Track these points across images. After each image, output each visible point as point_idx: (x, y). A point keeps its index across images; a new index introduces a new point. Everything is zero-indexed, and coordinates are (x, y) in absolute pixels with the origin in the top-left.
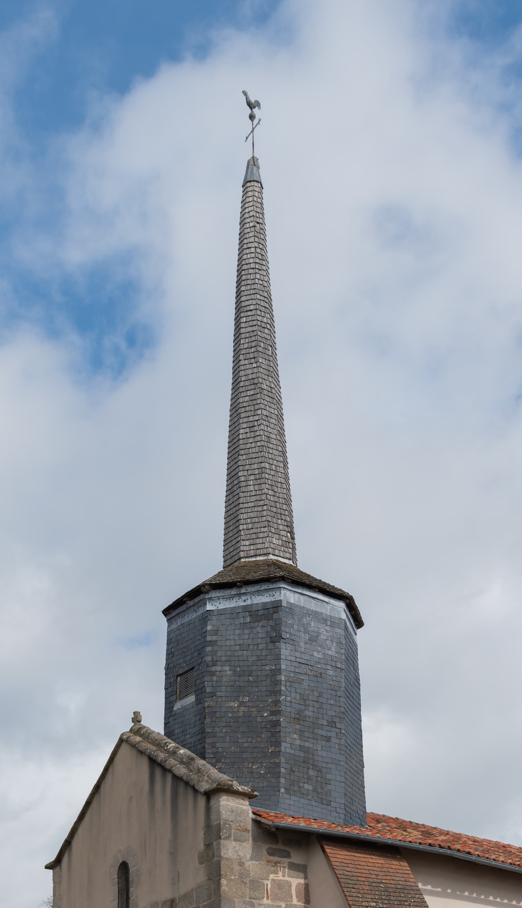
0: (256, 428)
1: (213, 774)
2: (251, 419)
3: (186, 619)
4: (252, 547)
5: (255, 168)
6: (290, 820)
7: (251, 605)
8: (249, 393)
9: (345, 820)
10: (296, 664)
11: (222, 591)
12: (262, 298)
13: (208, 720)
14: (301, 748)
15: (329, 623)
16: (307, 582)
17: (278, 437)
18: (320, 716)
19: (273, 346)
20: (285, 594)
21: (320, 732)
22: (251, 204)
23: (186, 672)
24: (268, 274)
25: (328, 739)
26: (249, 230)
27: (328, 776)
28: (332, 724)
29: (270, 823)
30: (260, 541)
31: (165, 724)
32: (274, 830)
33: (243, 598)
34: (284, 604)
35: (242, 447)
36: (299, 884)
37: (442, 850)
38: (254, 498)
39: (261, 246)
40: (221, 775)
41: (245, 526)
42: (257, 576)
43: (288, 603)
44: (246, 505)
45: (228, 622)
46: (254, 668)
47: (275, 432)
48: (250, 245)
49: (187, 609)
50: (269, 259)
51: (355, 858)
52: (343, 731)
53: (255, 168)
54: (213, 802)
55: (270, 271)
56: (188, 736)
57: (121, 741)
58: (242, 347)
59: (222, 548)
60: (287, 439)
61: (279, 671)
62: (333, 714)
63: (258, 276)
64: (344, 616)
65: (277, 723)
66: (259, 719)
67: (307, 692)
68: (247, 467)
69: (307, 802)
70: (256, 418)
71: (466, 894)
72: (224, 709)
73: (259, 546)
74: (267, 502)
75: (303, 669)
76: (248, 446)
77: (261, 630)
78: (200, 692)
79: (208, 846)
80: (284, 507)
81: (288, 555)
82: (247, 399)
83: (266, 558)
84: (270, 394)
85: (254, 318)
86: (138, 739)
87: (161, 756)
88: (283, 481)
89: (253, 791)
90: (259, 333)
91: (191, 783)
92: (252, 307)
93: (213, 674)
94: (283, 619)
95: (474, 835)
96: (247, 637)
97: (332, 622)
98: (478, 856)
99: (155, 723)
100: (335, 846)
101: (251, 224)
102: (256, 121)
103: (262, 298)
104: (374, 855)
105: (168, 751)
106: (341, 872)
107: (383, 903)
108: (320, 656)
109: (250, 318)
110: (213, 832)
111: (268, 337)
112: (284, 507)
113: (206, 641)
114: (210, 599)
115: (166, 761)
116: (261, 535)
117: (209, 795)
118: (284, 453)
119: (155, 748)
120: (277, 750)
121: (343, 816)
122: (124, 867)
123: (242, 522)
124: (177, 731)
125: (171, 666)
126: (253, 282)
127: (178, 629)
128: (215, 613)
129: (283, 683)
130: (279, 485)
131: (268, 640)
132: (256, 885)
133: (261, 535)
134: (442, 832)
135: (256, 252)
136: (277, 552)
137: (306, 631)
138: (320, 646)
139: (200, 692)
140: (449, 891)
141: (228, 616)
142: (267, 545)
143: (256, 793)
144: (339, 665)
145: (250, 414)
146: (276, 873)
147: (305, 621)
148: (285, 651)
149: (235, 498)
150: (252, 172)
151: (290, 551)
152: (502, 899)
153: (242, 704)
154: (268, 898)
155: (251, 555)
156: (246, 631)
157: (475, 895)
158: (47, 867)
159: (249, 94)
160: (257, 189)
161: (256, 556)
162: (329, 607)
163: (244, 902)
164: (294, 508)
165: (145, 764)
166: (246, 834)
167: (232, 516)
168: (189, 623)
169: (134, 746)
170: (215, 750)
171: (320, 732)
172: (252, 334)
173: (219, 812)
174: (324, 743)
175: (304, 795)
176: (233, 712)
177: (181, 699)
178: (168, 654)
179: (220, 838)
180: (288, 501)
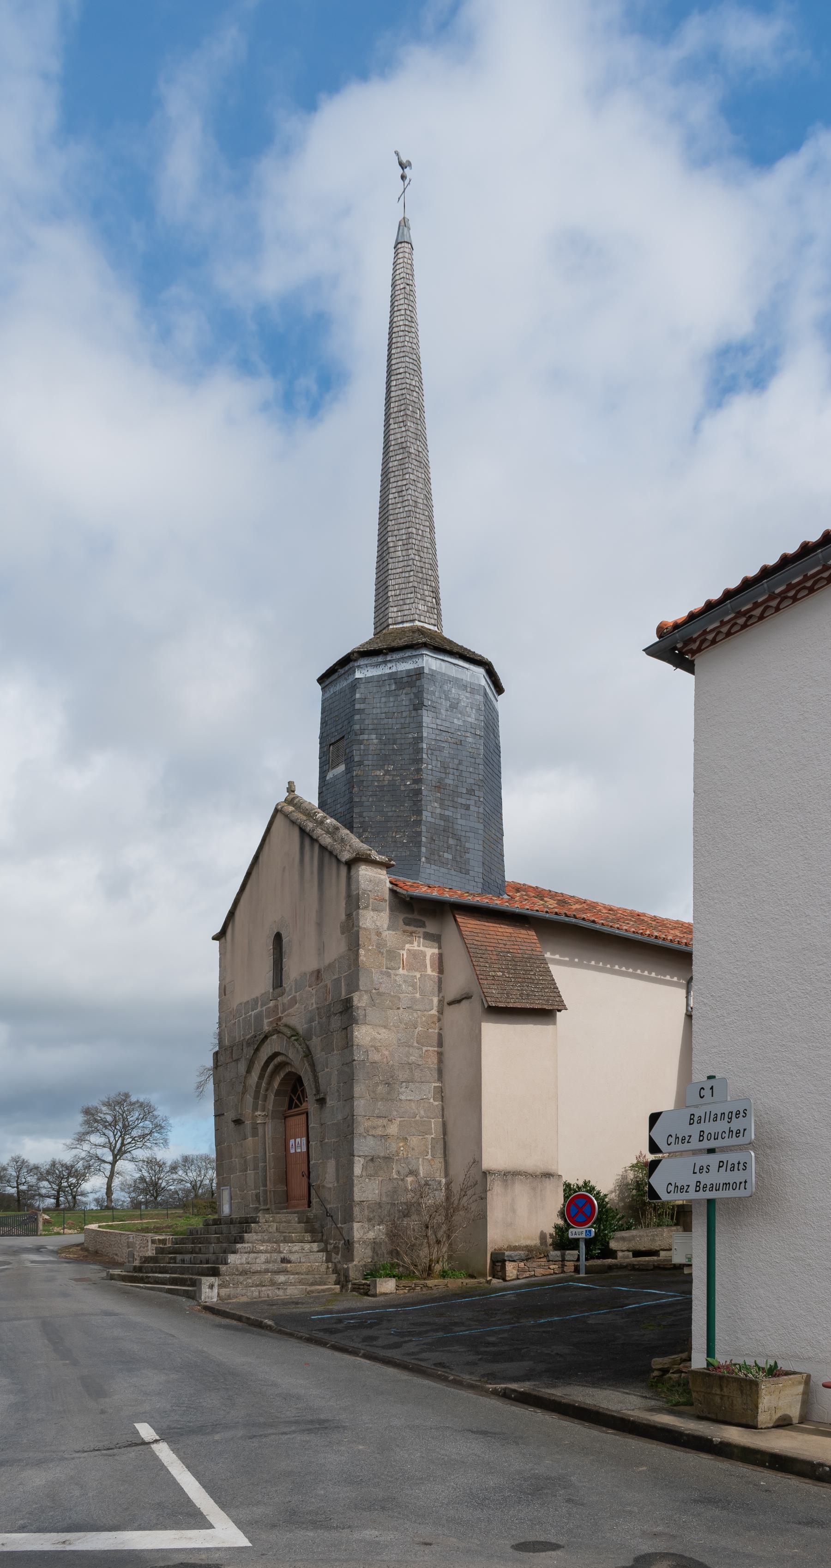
0: (404, 493)
1: (357, 843)
2: (400, 483)
3: (338, 687)
4: (399, 614)
5: (406, 229)
6: (425, 889)
7: (396, 672)
8: (398, 457)
9: (483, 889)
10: (437, 732)
11: (370, 658)
12: (411, 361)
13: (356, 789)
14: (442, 817)
15: (469, 689)
16: (448, 648)
17: (425, 502)
18: (460, 784)
19: (421, 409)
20: (427, 661)
21: (460, 800)
22: (402, 265)
23: (337, 741)
24: (417, 337)
25: (467, 807)
26: (399, 292)
27: (467, 845)
28: (471, 792)
29: (404, 892)
30: (407, 607)
31: (319, 794)
32: (408, 899)
33: (389, 665)
34: (426, 671)
35: (391, 512)
36: (433, 954)
37: (567, 919)
38: (401, 564)
39: (410, 308)
40: (361, 844)
41: (393, 593)
42: (401, 642)
43: (430, 669)
44: (394, 571)
45: (375, 690)
46: (398, 736)
47: (422, 496)
48: (400, 307)
49: (339, 677)
50: (418, 322)
51: (484, 928)
52: (482, 799)
53: (406, 229)
54: (353, 872)
55: (419, 333)
56: (339, 806)
57: (276, 811)
58: (392, 410)
59: (373, 615)
60: (434, 503)
61: (420, 739)
62: (473, 782)
63: (407, 338)
64: (483, 682)
65: (418, 792)
66: (402, 788)
67: (448, 760)
68: (396, 533)
69: (446, 871)
70: (405, 482)
71: (593, 963)
72: (370, 778)
73: (406, 613)
74: (414, 568)
75: (444, 736)
76: (397, 511)
77: (404, 698)
78: (349, 761)
79: (349, 916)
80: (430, 572)
81: (433, 621)
82: (396, 463)
83: (411, 624)
84: (418, 458)
85: (403, 381)
86: (291, 808)
87: (310, 825)
88: (429, 546)
89: (390, 860)
90: (408, 396)
91: (335, 853)
92: (401, 370)
93: (361, 742)
94: (425, 686)
95: (611, 904)
96: (392, 704)
97: (472, 689)
98: (603, 924)
99: (310, 795)
100: (466, 916)
101: (402, 286)
102: (407, 181)
103: (411, 361)
104: (503, 924)
105: (316, 821)
106: (471, 942)
107: (509, 973)
108: (460, 723)
109: (399, 382)
110: (354, 902)
111: (416, 400)
112: (430, 572)
113: (354, 710)
114: (359, 667)
115: (313, 831)
116: (408, 601)
117: (351, 864)
118: (430, 518)
119: (304, 818)
120: (419, 818)
121: (480, 885)
122: (278, 937)
123: (390, 588)
124: (329, 801)
125: (325, 735)
126: (402, 344)
127: (331, 697)
128: (364, 681)
129: (425, 751)
130: (425, 550)
131: (411, 707)
132: (392, 955)
133: (408, 601)
134: (579, 901)
135: (406, 314)
136: (422, 618)
137: (447, 698)
138: (461, 713)
139: (349, 761)
140: (576, 960)
141: (375, 684)
142: (413, 611)
143: (393, 862)
144: (478, 732)
145: (398, 478)
146: (411, 943)
147: (446, 688)
148: (427, 718)
149: (385, 564)
150: (403, 233)
151: (435, 617)
152: (627, 968)
153: (387, 772)
154: (403, 969)
155: (401, 620)
156: (392, 699)
157: (601, 964)
158: (214, 938)
159: (401, 155)
160: (407, 250)
161: (403, 622)
162: (469, 673)
163: (381, 973)
164: (440, 573)
165: (296, 833)
166: (383, 904)
167: (382, 583)
168: (341, 691)
169: (287, 816)
170: (362, 819)
171: (460, 800)
172: (401, 398)
173: (358, 882)
174: (463, 811)
175: (443, 864)
176: (378, 781)
177: (333, 768)
178: (322, 724)
179: (359, 908)
180: (434, 567)
